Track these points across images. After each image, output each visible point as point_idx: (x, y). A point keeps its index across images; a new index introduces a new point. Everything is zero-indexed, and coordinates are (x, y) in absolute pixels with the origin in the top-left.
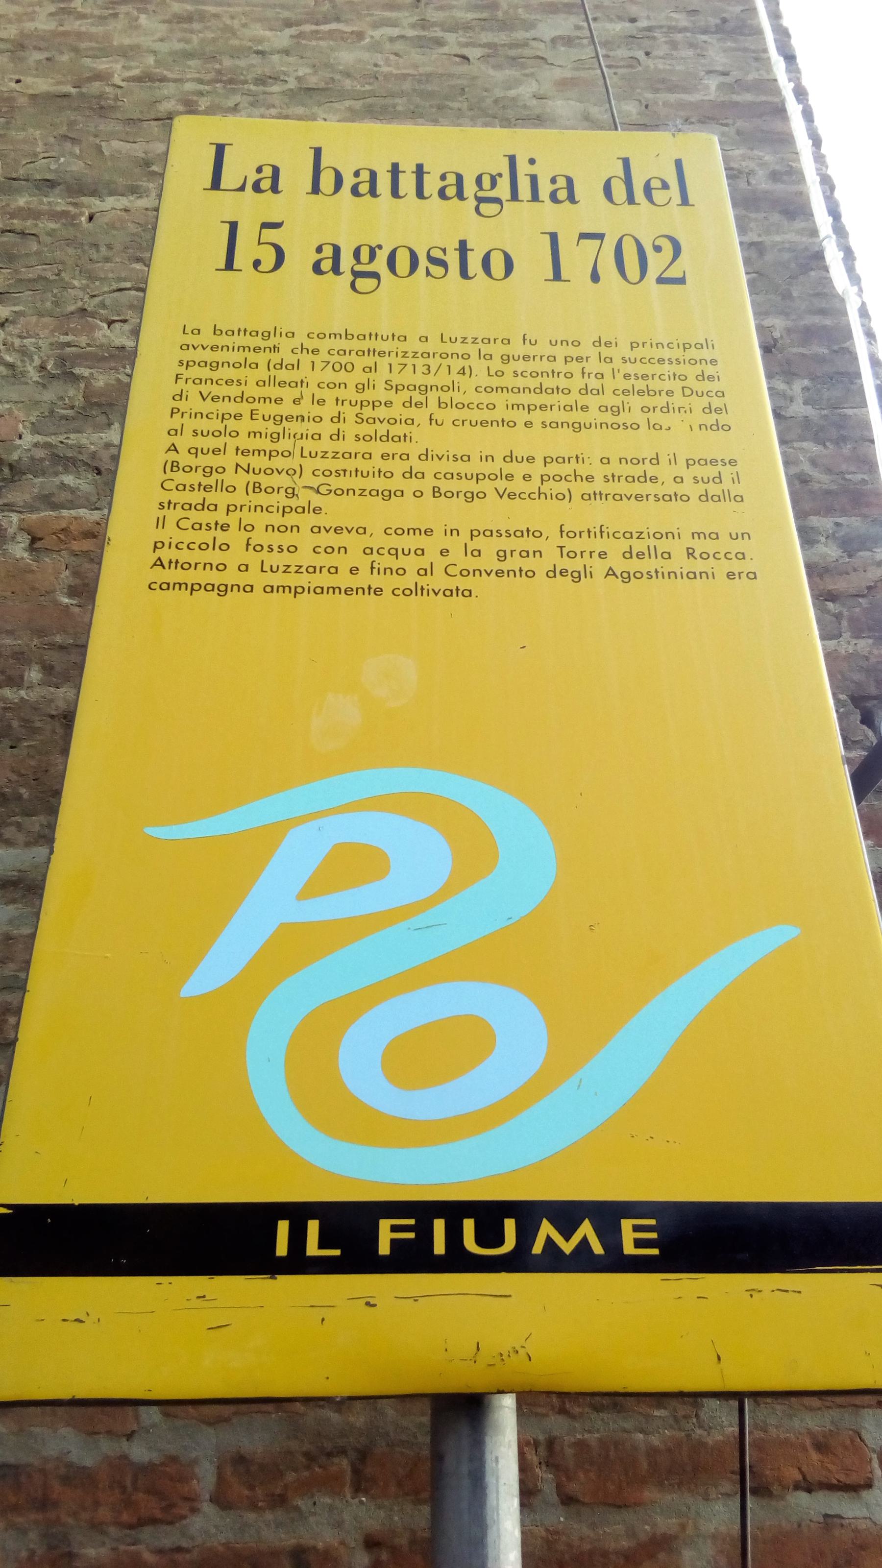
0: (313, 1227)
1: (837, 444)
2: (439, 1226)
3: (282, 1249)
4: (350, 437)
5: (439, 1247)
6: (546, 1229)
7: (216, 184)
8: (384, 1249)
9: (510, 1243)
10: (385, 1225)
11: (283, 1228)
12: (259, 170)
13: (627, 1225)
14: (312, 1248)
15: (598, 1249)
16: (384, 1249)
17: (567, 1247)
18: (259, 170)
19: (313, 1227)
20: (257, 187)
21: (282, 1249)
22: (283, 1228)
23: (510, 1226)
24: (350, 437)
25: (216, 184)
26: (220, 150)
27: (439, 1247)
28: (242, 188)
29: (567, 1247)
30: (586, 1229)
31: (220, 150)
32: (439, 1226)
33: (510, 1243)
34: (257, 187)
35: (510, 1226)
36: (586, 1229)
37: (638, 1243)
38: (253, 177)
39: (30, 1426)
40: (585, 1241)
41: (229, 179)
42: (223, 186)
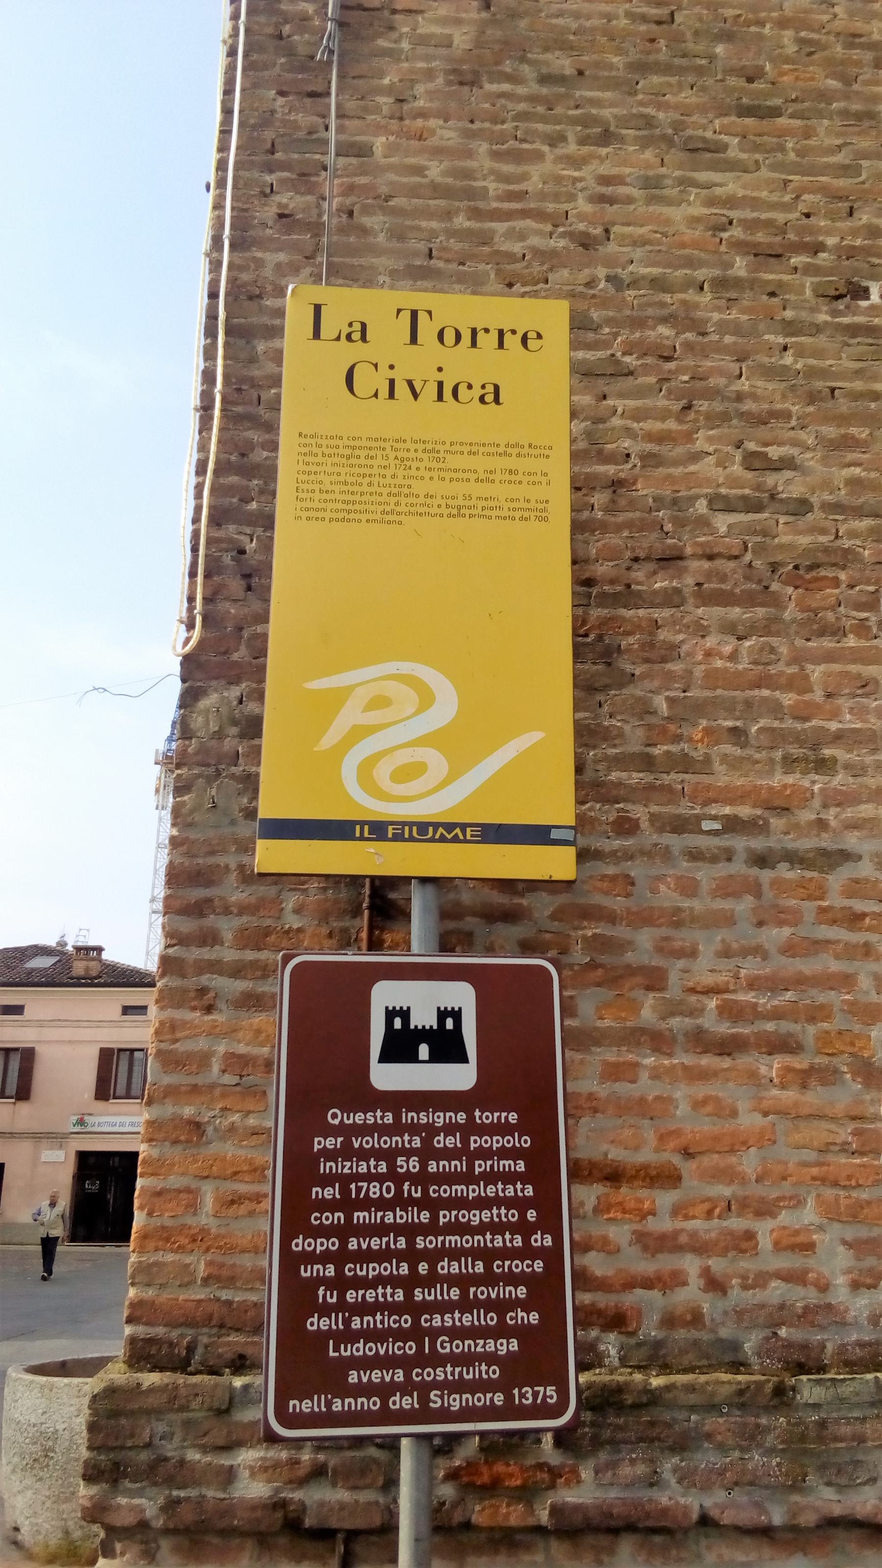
0: (366, 828)
1: (856, 1322)
2: (407, 828)
3: (358, 834)
4: (400, 477)
5: (407, 836)
6: (441, 830)
7: (317, 335)
8: (390, 835)
9: (430, 834)
10: (390, 828)
11: (358, 827)
12: (350, 325)
13: (468, 830)
14: (366, 835)
15: (461, 837)
16: (390, 835)
17: (449, 837)
18: (350, 325)
19: (366, 828)
20: (349, 337)
21: (358, 834)
22: (358, 827)
23: (431, 829)
24: (400, 477)
25: (317, 335)
26: (318, 309)
27: (407, 836)
28: (338, 338)
29: (449, 837)
30: (458, 831)
31: (318, 309)
32: (407, 828)
33: (430, 834)
34: (349, 337)
35: (431, 829)
36: (458, 831)
37: (472, 836)
38: (346, 330)
39: (59, 961)
40: (456, 835)
41: (326, 331)
42: (322, 336)
